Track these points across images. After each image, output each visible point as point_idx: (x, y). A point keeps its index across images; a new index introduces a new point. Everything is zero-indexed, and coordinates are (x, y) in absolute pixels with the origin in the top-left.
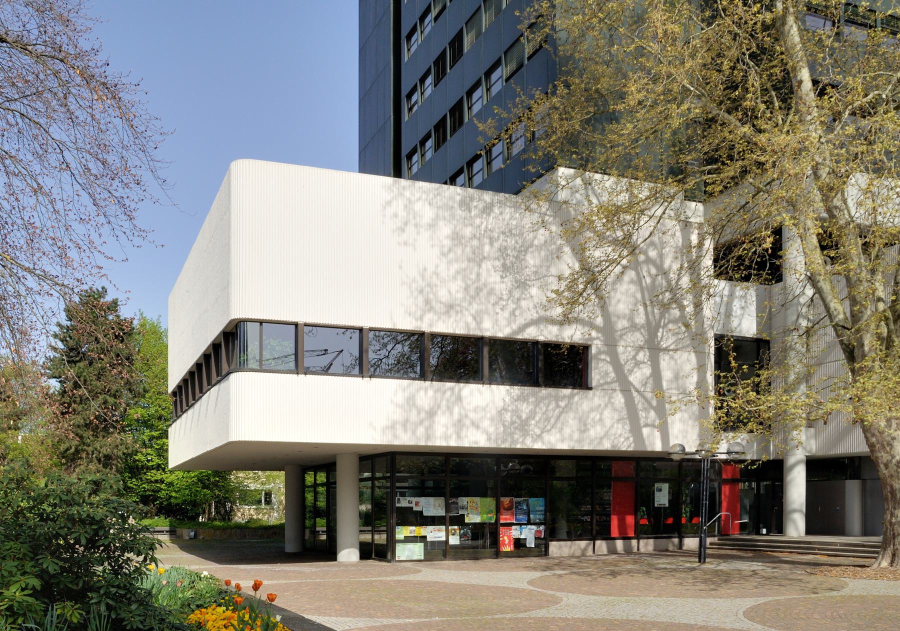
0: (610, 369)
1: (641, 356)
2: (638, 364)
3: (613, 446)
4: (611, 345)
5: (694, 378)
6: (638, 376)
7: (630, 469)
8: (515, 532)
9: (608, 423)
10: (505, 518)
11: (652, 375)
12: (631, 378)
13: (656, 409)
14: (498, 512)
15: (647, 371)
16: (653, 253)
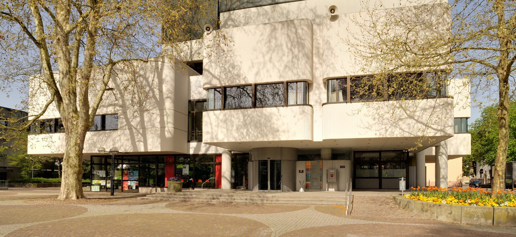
0: (124, 120)
1: (136, 114)
2: (135, 117)
3: (125, 150)
4: (125, 113)
5: (158, 119)
6: (134, 123)
7: (136, 158)
8: (129, 183)
9: (123, 141)
10: (125, 178)
11: (140, 121)
12: (132, 123)
13: (141, 134)
14: (122, 175)
15: (138, 119)
16: (142, 72)
